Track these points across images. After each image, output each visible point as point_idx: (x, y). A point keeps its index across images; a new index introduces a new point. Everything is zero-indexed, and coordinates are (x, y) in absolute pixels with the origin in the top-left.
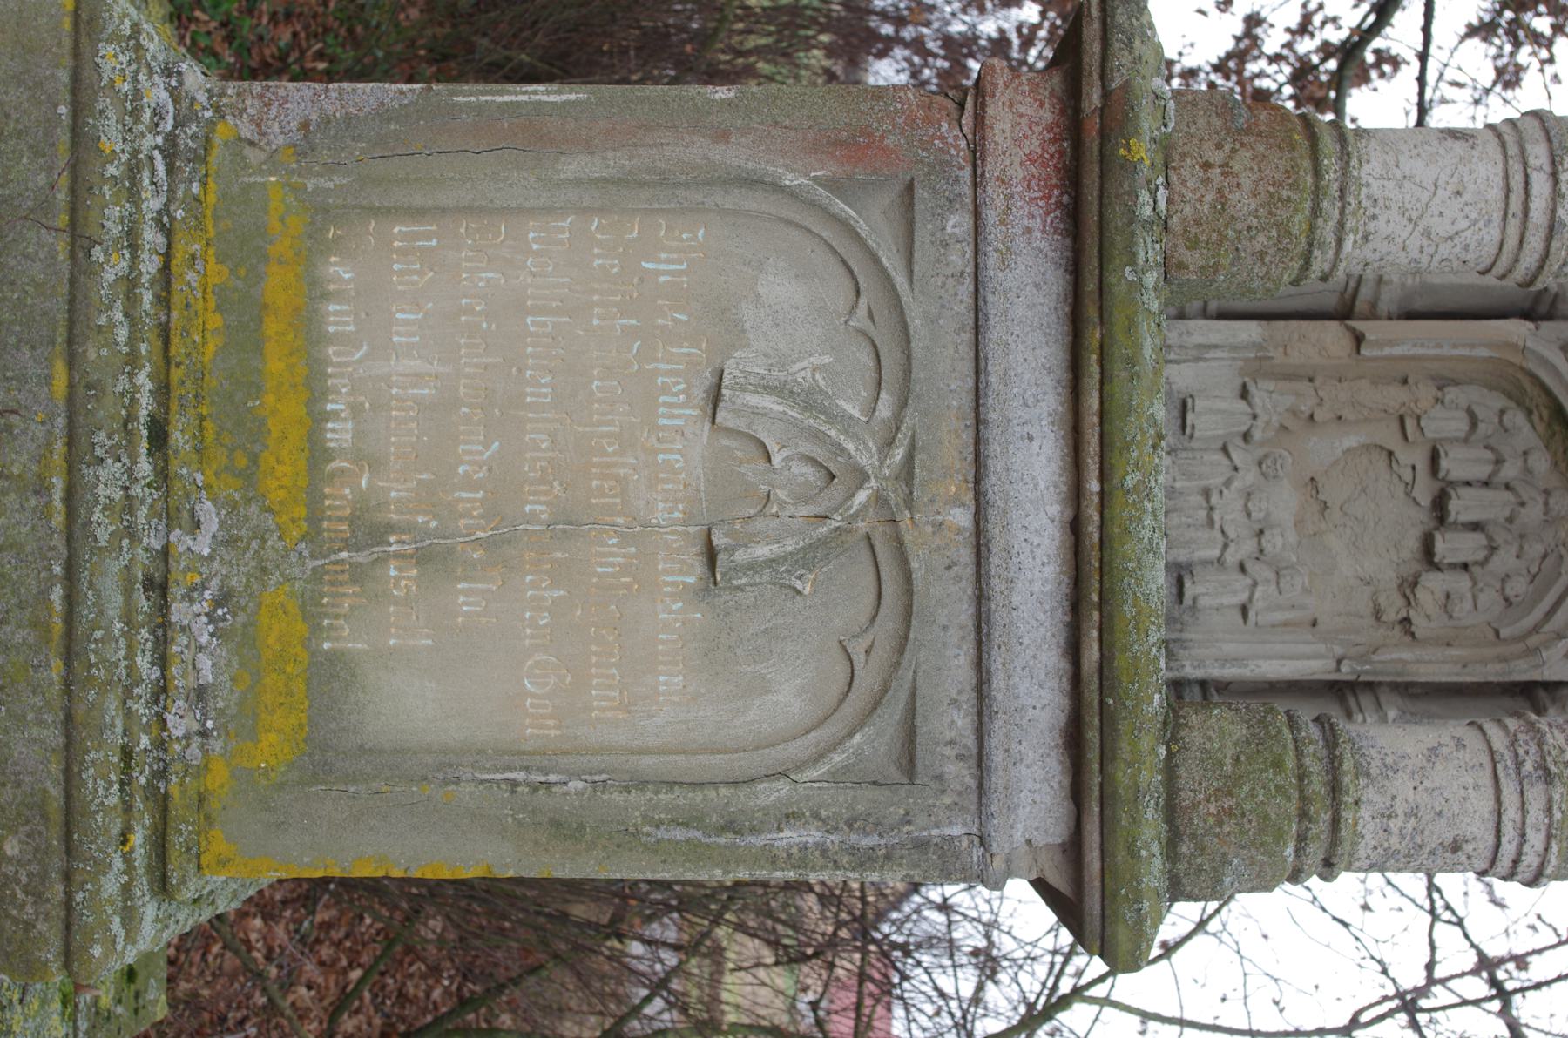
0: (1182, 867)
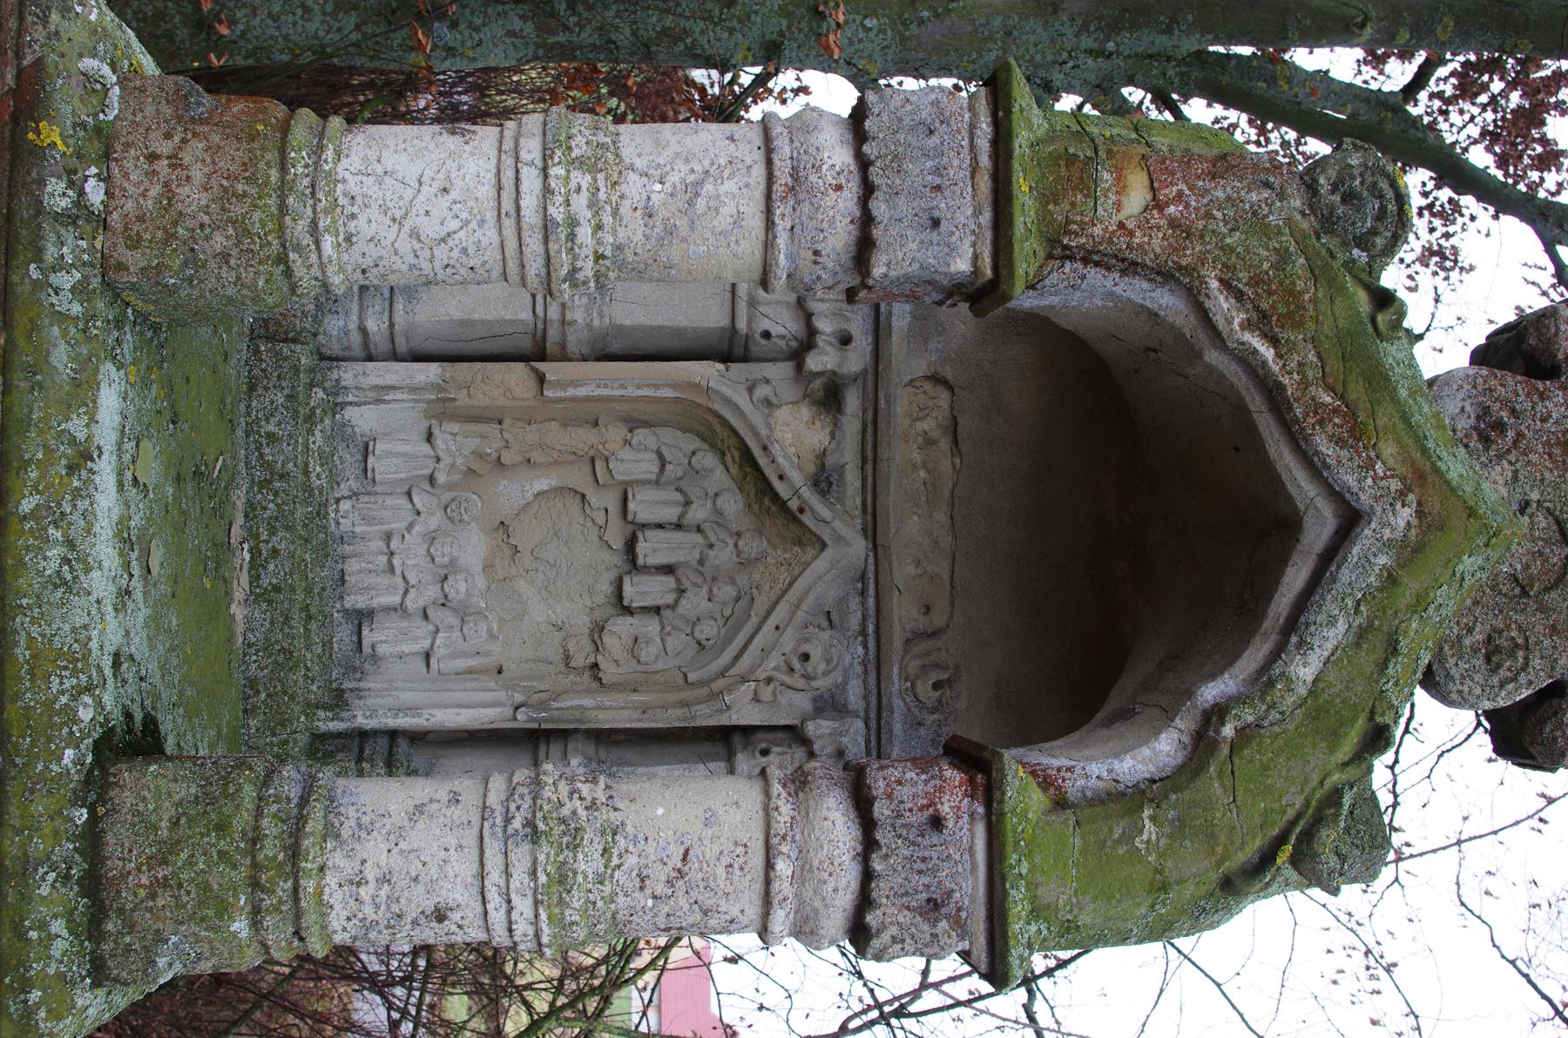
0: (107, 947)
